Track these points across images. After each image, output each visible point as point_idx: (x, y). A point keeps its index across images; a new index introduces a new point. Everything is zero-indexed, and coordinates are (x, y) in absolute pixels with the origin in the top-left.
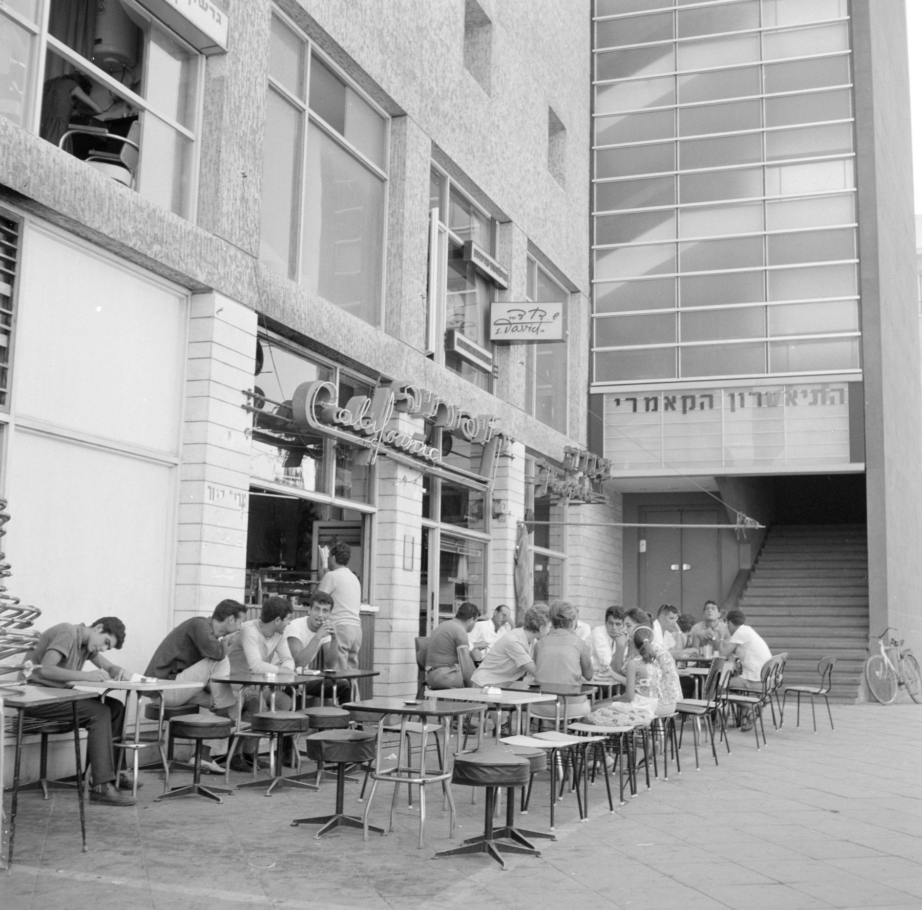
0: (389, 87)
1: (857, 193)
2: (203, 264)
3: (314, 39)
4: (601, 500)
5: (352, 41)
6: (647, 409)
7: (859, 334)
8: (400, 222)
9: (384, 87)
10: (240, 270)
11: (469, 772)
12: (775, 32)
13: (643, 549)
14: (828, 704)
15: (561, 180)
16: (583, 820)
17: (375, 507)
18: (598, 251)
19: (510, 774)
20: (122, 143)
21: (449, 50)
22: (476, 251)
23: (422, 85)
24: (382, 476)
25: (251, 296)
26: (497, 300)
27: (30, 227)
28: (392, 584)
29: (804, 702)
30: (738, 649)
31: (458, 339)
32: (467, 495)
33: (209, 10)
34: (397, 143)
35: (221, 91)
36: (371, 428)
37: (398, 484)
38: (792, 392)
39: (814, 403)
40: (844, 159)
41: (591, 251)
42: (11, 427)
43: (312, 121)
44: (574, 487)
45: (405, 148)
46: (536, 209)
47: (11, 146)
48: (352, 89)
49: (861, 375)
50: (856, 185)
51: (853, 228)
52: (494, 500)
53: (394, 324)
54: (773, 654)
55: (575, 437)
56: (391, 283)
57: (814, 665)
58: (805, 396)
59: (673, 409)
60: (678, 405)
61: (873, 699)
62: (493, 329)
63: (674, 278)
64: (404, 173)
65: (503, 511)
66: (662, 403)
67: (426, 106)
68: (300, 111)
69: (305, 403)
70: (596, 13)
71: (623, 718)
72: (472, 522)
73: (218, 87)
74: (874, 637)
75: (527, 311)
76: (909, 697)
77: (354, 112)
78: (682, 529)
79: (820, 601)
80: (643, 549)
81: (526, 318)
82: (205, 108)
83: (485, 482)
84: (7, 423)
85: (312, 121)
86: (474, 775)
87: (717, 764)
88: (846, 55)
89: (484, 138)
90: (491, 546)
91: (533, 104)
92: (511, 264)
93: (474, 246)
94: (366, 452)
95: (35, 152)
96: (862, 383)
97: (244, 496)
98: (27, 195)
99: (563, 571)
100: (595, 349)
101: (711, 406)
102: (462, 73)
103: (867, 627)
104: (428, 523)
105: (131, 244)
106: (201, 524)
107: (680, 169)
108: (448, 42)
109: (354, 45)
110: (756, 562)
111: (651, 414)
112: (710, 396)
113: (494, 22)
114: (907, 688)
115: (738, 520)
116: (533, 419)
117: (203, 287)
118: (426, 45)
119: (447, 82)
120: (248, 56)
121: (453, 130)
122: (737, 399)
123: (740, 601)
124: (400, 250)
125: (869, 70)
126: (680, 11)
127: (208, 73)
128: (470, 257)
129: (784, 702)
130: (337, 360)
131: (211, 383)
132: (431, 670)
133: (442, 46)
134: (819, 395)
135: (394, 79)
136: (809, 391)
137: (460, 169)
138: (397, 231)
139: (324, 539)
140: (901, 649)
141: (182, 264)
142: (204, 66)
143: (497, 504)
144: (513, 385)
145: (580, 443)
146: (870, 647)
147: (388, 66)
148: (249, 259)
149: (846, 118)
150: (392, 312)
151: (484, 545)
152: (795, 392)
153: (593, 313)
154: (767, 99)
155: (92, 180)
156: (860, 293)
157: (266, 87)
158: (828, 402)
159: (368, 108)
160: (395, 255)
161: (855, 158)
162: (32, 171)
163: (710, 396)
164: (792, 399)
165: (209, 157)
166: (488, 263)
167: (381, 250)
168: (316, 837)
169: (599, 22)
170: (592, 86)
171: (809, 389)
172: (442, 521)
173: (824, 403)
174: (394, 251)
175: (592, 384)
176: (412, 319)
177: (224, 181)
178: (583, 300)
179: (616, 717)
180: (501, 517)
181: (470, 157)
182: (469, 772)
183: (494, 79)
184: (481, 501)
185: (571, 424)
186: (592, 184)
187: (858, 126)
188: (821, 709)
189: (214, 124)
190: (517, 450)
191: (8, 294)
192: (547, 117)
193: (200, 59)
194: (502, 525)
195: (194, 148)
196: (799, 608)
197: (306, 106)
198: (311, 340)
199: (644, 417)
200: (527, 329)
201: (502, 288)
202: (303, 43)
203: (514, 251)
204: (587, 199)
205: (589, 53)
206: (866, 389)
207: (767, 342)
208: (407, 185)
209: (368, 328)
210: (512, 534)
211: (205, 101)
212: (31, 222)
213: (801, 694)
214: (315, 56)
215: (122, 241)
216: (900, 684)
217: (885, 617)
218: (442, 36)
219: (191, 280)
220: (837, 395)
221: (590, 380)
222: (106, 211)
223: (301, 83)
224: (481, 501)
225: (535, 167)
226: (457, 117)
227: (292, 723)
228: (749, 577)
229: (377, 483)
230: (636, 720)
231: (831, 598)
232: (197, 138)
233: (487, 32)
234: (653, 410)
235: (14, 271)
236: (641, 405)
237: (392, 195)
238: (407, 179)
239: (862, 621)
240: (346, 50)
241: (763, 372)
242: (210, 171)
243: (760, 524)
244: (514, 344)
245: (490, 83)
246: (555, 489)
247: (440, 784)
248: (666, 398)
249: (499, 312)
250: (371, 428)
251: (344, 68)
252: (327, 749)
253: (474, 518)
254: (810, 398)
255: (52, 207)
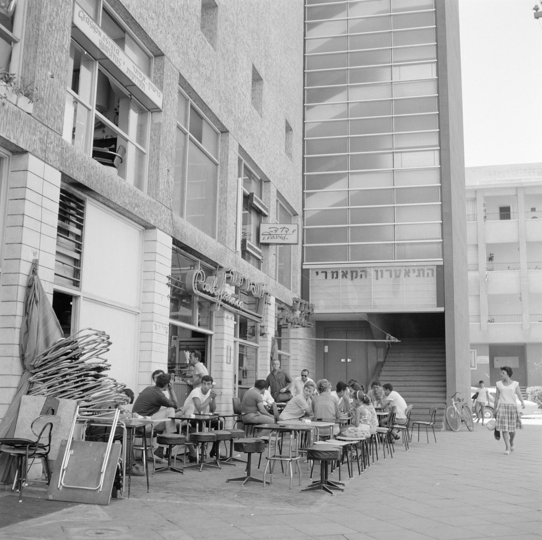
0: (222, 119)
1: (440, 168)
2: (153, 215)
3: (191, 98)
4: (309, 326)
5: (208, 98)
6: (333, 278)
7: (441, 240)
8: (226, 186)
9: (220, 119)
10: (166, 217)
11: (316, 454)
12: (399, 83)
13: (326, 350)
14: (427, 431)
15: (290, 157)
16: (351, 479)
17: (213, 331)
18: (307, 193)
19: (333, 455)
20: (115, 156)
21: (245, 97)
22: (255, 198)
23: (235, 116)
24: (216, 316)
25: (170, 229)
26: (262, 222)
27: (90, 204)
28: (222, 371)
29: (421, 431)
30: (391, 403)
31: (248, 244)
32: (247, 323)
33: (156, 92)
34: (224, 146)
35: (159, 129)
36: (217, 293)
37: (225, 320)
38: (407, 270)
39: (419, 276)
40: (434, 150)
41: (303, 193)
42: (82, 298)
43: (191, 139)
44: (298, 319)
45: (228, 148)
46: (280, 174)
47: (87, 166)
48: (205, 120)
49: (442, 262)
50: (440, 164)
51: (438, 186)
52: (261, 326)
53: (222, 238)
54: (408, 405)
55: (295, 292)
56: (221, 217)
57: (427, 411)
58: (414, 272)
59: (346, 277)
60: (349, 276)
61: (449, 428)
62: (261, 237)
63: (346, 209)
64: (228, 161)
65: (266, 332)
66: (340, 274)
67: (237, 127)
68: (185, 134)
69: (192, 281)
70: (306, 68)
71: (360, 434)
72: (249, 337)
73: (157, 128)
74: (449, 397)
75: (279, 228)
76: (467, 428)
77: (206, 133)
78: (347, 341)
79: (420, 378)
80: (326, 350)
81: (279, 232)
82: (151, 137)
83: (260, 318)
84: (79, 296)
85: (191, 139)
86: (319, 456)
87: (392, 457)
88: (435, 97)
89: (259, 139)
90: (259, 350)
91: (279, 119)
92: (270, 203)
93: (255, 196)
94: (214, 305)
95: (95, 168)
96: (443, 265)
97: (167, 328)
98: (92, 189)
99: (289, 363)
100: (305, 245)
101: (366, 277)
102: (251, 108)
103: (445, 392)
104: (236, 339)
105: (127, 209)
106: (152, 342)
107: (350, 152)
108: (245, 93)
109: (209, 100)
110: (386, 357)
111: (334, 280)
112: (364, 270)
113: (264, 80)
114: (466, 423)
115: (387, 338)
116: (277, 282)
117: (151, 226)
118: (237, 96)
119: (245, 113)
120: (170, 112)
121: (247, 137)
122: (379, 273)
123: (379, 378)
124: (225, 201)
125: (447, 105)
126: (350, 69)
127: (152, 121)
128: (252, 201)
129: (412, 430)
130: (199, 258)
131: (156, 273)
132: (245, 414)
133: (243, 95)
134: (421, 272)
135: (224, 115)
136: (416, 269)
137: (249, 156)
138: (224, 191)
139: (182, 347)
140: (462, 403)
141: (145, 216)
142: (150, 117)
143: (262, 329)
144: (270, 266)
145: (298, 295)
146: (447, 403)
147: (222, 108)
148: (169, 211)
149: (435, 129)
150: (221, 232)
151: (256, 349)
152: (409, 270)
153: (304, 226)
154: (395, 117)
155: (114, 179)
156: (442, 220)
157: (176, 126)
158: (426, 275)
159: (211, 129)
160: (223, 203)
161: (440, 150)
162: (94, 178)
163: (364, 270)
164: (407, 274)
165: (153, 162)
166: (259, 202)
167: (216, 201)
168: (243, 485)
169: (308, 73)
170: (304, 106)
171: (416, 269)
172: (240, 337)
173: (424, 276)
174: (222, 201)
175: (304, 264)
176: (230, 236)
177: (161, 174)
178: (300, 219)
179: (356, 433)
180: (264, 335)
181: (254, 150)
182: (316, 454)
183: (263, 109)
184: (254, 326)
185: (293, 284)
186: (303, 158)
187: (441, 133)
188: (431, 434)
189: (156, 146)
190: (272, 300)
191: (80, 235)
192: (285, 125)
193: (148, 114)
194: (265, 339)
195: (146, 157)
196: (410, 382)
197: (188, 132)
198: (191, 248)
199: (331, 281)
200: (279, 238)
201: (265, 216)
202: (187, 100)
203: (271, 196)
204: (301, 166)
205: (302, 89)
206: (445, 269)
207: (395, 244)
208: (229, 167)
209: (211, 238)
210: (269, 344)
211: (151, 134)
212: (89, 200)
213: (420, 425)
214: (192, 107)
215: (124, 207)
216: (462, 421)
217: (454, 387)
218: (243, 90)
219: (148, 223)
220: (430, 272)
221: (303, 261)
222: (119, 193)
223: (186, 120)
224: (254, 326)
225: (280, 152)
226: (249, 130)
227: (210, 438)
228: (382, 366)
229: (214, 319)
230: (365, 435)
231: (425, 377)
232: (147, 152)
233: (260, 84)
234: (336, 278)
235: (83, 223)
236: (329, 275)
237: (221, 172)
238: (229, 165)
239: (443, 389)
240: (206, 103)
241: (393, 259)
242: (154, 169)
243: (398, 340)
244: (271, 245)
245: (261, 111)
246: (289, 320)
247: (295, 461)
248: (343, 272)
249: (264, 228)
250: (217, 293)
251: (203, 111)
252: (246, 446)
253: (250, 336)
254: (417, 273)
255: (100, 194)
